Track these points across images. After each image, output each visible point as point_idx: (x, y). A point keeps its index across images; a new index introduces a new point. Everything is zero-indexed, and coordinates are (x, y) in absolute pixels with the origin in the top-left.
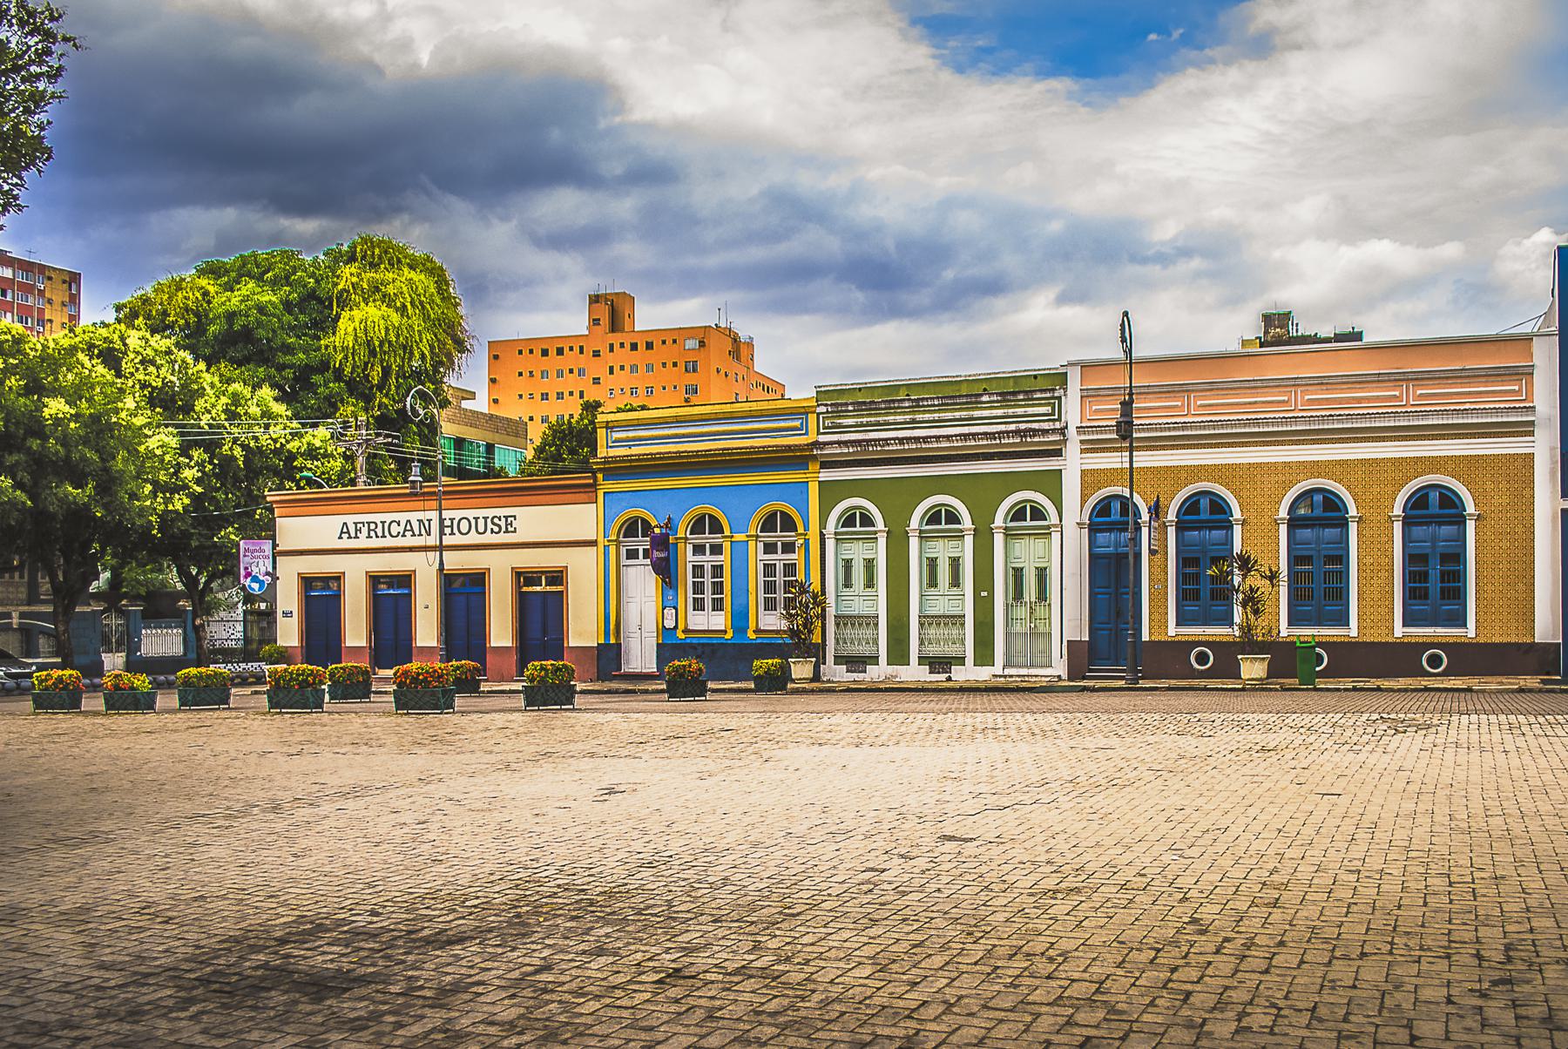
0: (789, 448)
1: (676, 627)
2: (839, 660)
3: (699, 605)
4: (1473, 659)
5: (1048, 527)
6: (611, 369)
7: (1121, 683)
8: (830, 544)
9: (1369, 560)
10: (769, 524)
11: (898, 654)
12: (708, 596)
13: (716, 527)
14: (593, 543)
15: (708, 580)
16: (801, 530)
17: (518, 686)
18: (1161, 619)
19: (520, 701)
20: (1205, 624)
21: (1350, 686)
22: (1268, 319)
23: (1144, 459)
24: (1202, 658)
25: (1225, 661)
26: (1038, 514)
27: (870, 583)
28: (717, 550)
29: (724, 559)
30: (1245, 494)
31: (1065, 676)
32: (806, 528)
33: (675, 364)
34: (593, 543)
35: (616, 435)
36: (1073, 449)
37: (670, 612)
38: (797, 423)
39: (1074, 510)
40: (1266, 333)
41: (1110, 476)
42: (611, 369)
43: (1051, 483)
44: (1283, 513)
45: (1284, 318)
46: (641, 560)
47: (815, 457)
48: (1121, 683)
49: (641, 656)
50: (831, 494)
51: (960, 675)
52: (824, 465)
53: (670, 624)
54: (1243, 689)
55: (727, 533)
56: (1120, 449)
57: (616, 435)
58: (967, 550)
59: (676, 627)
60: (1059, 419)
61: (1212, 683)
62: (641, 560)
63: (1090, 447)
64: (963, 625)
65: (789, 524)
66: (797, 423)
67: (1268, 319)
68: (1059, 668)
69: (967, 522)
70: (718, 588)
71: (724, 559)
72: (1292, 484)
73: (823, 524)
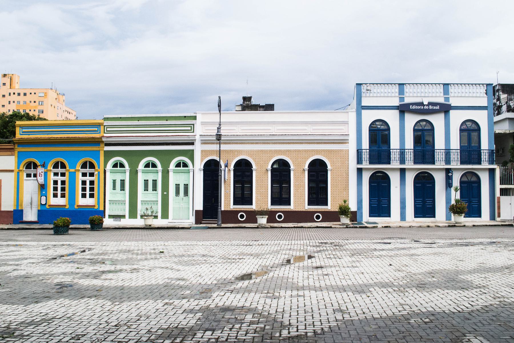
0: (93, 138)
1: (46, 204)
2: (110, 216)
3: (55, 196)
4: (331, 217)
5: (189, 170)
6: (10, 102)
7: (215, 225)
8: (108, 174)
9: (297, 183)
10: (84, 166)
11: (133, 214)
12: (59, 192)
13: (63, 166)
14: (12, 171)
15: (59, 186)
16: (97, 168)
17: (52, 226)
18: (227, 201)
19: (52, 232)
20: (280, 204)
21: (293, 226)
22: (245, 99)
23: (224, 147)
24: (280, 217)
25: (252, 217)
26: (185, 165)
27: (123, 188)
28: (92, 175)
29: (66, 178)
30: (257, 160)
31: (194, 223)
32: (99, 168)
33: (35, 102)
34: (12, 171)
35: (24, 130)
36: (198, 143)
37: (44, 198)
38: (96, 129)
39: (199, 164)
40: (244, 103)
41: (211, 152)
42: (10, 102)
43: (190, 154)
44: (269, 167)
45: (249, 99)
46: (32, 178)
47: (103, 142)
48: (215, 225)
49: (30, 215)
50: (109, 155)
51: (123, 223)
52: (107, 145)
53: (43, 202)
54: (257, 228)
55: (68, 168)
56: (217, 143)
57: (24, 130)
58: (159, 178)
59: (46, 204)
60: (193, 132)
61: (284, 225)
62: (32, 178)
63: (204, 142)
64: (157, 204)
65: (92, 166)
66: (96, 129)
67: (245, 99)
68: (192, 220)
69: (159, 167)
70: (63, 189)
71: (66, 178)
72: (272, 157)
73: (105, 166)
